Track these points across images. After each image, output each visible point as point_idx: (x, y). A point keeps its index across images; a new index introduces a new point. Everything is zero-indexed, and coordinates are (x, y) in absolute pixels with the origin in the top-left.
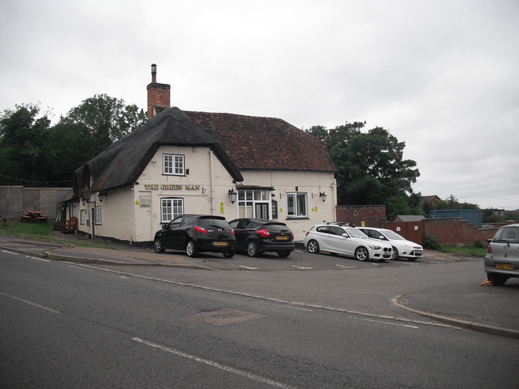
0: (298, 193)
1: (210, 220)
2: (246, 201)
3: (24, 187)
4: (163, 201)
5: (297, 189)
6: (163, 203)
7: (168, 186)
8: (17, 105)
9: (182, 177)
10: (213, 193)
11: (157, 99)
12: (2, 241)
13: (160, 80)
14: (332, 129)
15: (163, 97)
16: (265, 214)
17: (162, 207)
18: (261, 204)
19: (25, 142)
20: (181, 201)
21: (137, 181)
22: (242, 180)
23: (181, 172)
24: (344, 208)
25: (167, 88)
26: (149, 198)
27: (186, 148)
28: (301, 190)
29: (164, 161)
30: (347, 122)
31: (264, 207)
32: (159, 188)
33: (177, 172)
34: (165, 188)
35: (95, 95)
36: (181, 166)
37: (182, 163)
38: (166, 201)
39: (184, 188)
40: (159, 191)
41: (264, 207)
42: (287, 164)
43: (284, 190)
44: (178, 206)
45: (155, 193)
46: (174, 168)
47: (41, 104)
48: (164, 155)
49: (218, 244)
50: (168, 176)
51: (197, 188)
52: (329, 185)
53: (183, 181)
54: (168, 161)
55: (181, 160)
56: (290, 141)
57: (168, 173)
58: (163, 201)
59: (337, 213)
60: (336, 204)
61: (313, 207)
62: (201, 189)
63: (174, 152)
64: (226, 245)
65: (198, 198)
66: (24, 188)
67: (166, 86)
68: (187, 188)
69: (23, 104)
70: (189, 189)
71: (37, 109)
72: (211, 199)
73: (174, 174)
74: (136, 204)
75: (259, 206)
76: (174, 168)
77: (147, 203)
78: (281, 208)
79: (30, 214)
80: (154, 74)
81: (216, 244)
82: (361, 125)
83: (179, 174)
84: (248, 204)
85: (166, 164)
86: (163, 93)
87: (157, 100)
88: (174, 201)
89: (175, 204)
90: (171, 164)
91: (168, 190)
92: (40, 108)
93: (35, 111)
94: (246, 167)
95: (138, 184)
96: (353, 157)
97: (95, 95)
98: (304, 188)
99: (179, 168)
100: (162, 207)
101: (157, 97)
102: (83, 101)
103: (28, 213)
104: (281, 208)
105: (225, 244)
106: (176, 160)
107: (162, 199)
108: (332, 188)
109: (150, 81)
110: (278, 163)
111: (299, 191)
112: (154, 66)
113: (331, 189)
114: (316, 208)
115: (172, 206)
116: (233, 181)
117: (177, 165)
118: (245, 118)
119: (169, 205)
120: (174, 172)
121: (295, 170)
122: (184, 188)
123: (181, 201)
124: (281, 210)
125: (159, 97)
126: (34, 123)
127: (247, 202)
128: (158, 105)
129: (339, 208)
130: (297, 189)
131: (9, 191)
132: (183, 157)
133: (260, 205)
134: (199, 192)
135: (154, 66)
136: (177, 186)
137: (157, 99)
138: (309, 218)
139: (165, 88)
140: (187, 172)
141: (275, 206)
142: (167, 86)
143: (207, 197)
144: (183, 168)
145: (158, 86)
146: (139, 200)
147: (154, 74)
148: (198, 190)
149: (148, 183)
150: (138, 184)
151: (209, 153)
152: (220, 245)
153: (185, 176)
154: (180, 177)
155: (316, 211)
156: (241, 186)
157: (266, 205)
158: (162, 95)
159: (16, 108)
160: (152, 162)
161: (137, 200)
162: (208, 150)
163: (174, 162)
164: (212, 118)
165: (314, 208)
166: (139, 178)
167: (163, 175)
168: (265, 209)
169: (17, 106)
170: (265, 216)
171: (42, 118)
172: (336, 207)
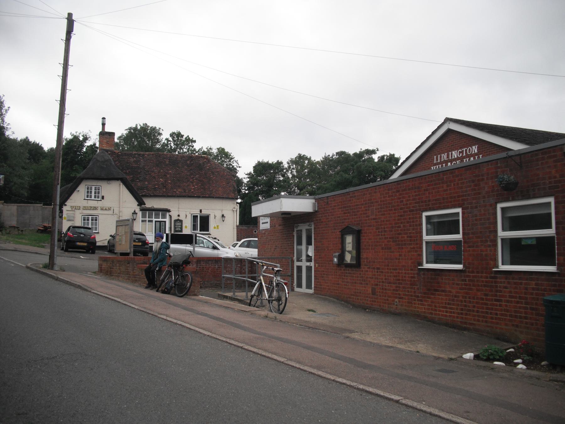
0: (201, 215)
1: (82, 229)
2: (147, 219)
3: (43, 205)
4: (84, 217)
5: (201, 211)
6: (193, 224)
7: (87, 207)
8: (72, 133)
9: (99, 201)
10: (121, 213)
11: (103, 143)
12: (4, 246)
13: (107, 129)
14: (266, 161)
15: (108, 142)
16: (163, 229)
17: (83, 221)
18: (160, 222)
19: (74, 167)
20: (97, 217)
21: (66, 203)
22: (145, 204)
23: (98, 198)
24: (244, 227)
25: (112, 135)
26: (73, 215)
27: (103, 181)
28: (205, 212)
29: (86, 190)
30: (361, 149)
31: (163, 224)
32: (81, 208)
33: (95, 197)
34: (85, 208)
35: (137, 125)
36: (99, 193)
37: (99, 192)
38: (85, 217)
39: (99, 208)
40: (80, 211)
41: (163, 224)
42: (193, 192)
43: (189, 212)
44: (86, 221)
45: (78, 212)
46: (93, 195)
47: (91, 132)
48: (86, 186)
49: (80, 244)
50: (88, 200)
51: (109, 209)
52: (231, 209)
53: (99, 204)
54: (89, 190)
55: (99, 190)
56: (205, 174)
57: (89, 199)
58: (84, 217)
59: (237, 231)
60: (238, 224)
61: (215, 226)
62: (112, 210)
63: (94, 184)
64: (86, 245)
65: (110, 216)
66: (43, 206)
67: (111, 134)
68: (102, 209)
69: (76, 132)
70: (103, 210)
71: (88, 137)
72: (120, 216)
73: (93, 199)
74: (64, 219)
75: (158, 224)
76: (93, 195)
77: (72, 218)
78: (186, 225)
79: (45, 227)
80: (103, 125)
81: (78, 244)
82: (373, 152)
83: (97, 199)
84: (149, 221)
85: (88, 192)
86: (109, 139)
87: (104, 144)
88: (92, 217)
89: (92, 220)
90: (91, 192)
91: (87, 210)
92: (90, 136)
93: (86, 139)
94: (157, 194)
95: (66, 205)
96: (356, 182)
97: (137, 125)
98: (208, 211)
99: (97, 195)
100: (83, 221)
101: (104, 142)
102: (126, 130)
103: (43, 226)
104: (186, 225)
105: (85, 244)
106: (95, 189)
107: (83, 216)
108: (234, 211)
109: (101, 130)
110: (185, 192)
111: (202, 213)
112: (104, 118)
113: (233, 212)
114: (218, 226)
115: (90, 221)
116: (138, 204)
117: (95, 193)
118: (174, 156)
119: (88, 220)
120: (93, 198)
121: (198, 197)
122: (99, 208)
123: (97, 217)
124: (186, 227)
125: (105, 142)
126: (84, 150)
127: (148, 220)
128: (105, 148)
129: (240, 227)
130: (201, 211)
131: (32, 208)
132: (100, 187)
133: (159, 222)
134: (111, 212)
135: (104, 118)
136: (94, 207)
137: (103, 143)
138: (211, 234)
139: (111, 135)
140: (103, 198)
141: (181, 224)
142: (112, 134)
143: (116, 216)
144: (100, 195)
145: (104, 134)
146: (66, 216)
147: (103, 125)
148: (110, 211)
149: (73, 204)
150: (66, 205)
151: (120, 185)
152: (81, 244)
153: (101, 200)
154: (97, 201)
155: (218, 228)
156: (153, 208)
157: (164, 223)
158: (108, 140)
159: (71, 135)
160: (77, 191)
161: (65, 216)
162: (119, 182)
163: (93, 191)
164: (146, 157)
165: (216, 226)
166: (67, 202)
167: (85, 199)
168: (163, 226)
169: (72, 134)
170: (163, 231)
171: (91, 145)
172: (237, 226)
